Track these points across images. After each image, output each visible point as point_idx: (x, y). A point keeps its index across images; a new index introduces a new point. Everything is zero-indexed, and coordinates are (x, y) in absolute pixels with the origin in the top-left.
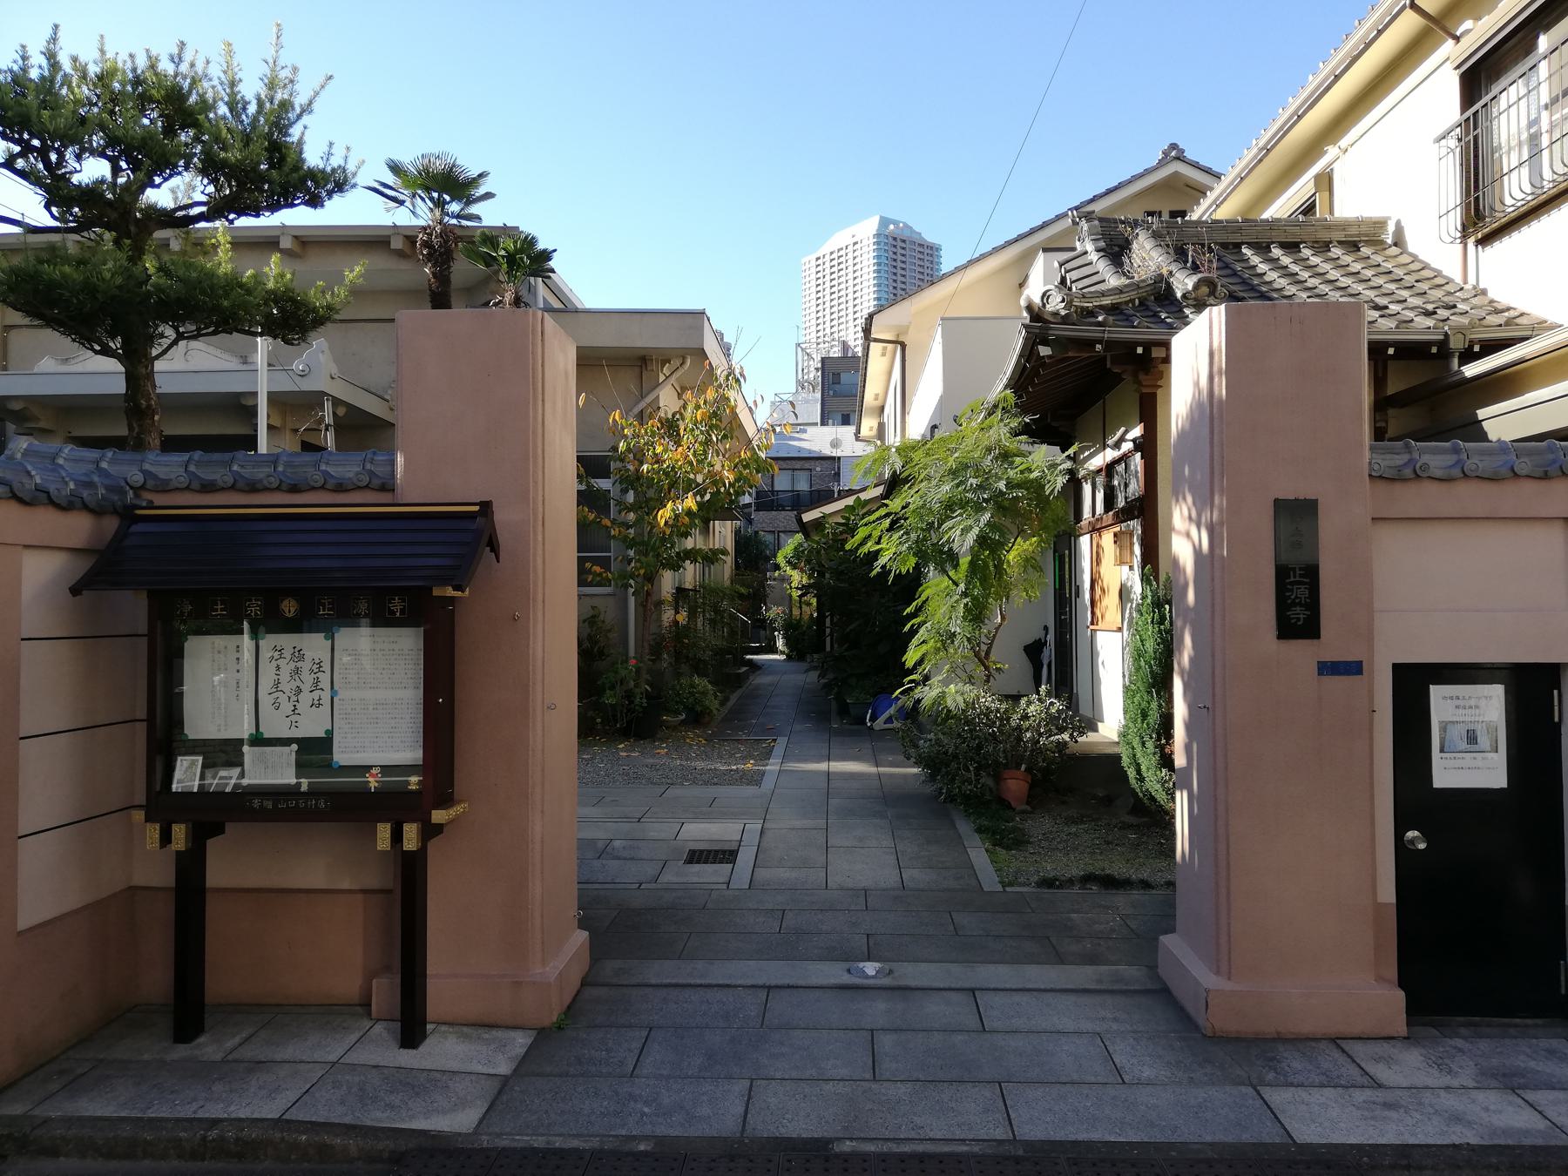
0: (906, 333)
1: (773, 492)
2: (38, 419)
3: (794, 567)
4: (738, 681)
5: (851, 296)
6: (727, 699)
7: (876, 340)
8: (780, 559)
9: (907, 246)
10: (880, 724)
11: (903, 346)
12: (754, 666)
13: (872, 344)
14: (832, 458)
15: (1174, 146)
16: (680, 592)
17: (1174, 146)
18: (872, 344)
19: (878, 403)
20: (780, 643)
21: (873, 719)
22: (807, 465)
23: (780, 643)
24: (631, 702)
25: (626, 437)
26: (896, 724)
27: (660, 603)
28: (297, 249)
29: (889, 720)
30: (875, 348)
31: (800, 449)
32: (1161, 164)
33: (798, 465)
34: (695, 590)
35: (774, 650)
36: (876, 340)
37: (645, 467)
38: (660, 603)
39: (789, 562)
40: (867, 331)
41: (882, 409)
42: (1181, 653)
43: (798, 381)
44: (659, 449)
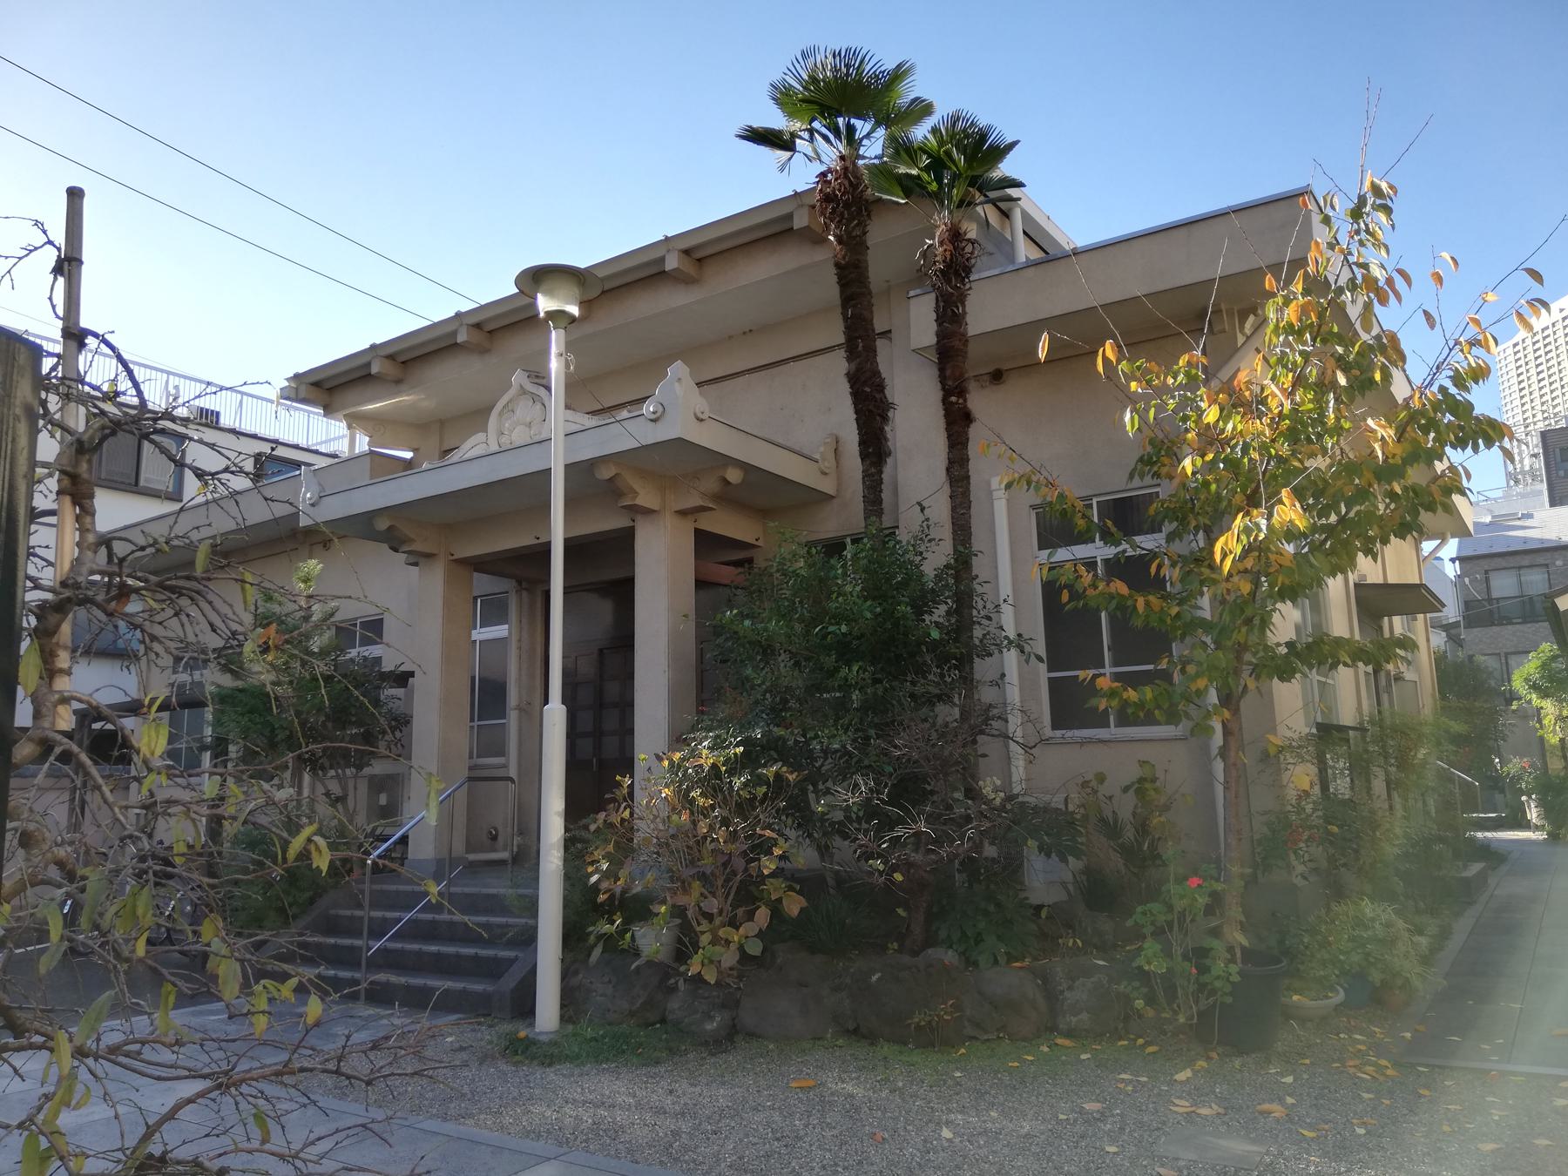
1: (1490, 600)
2: (411, 541)
3: (1545, 694)
4: (1467, 892)
6: (1445, 934)
8: (1518, 684)
12: (1492, 855)
16: (1328, 733)
20: (1533, 814)
22: (1540, 559)
23: (1533, 814)
24: (1203, 970)
25: (1132, 399)
27: (1270, 759)
28: (689, 268)
31: (1525, 540)
33: (1526, 561)
34: (1361, 729)
35: (1524, 824)
37: (1187, 464)
38: (1270, 759)
39: (1535, 687)
43: (1508, 475)
44: (1211, 415)
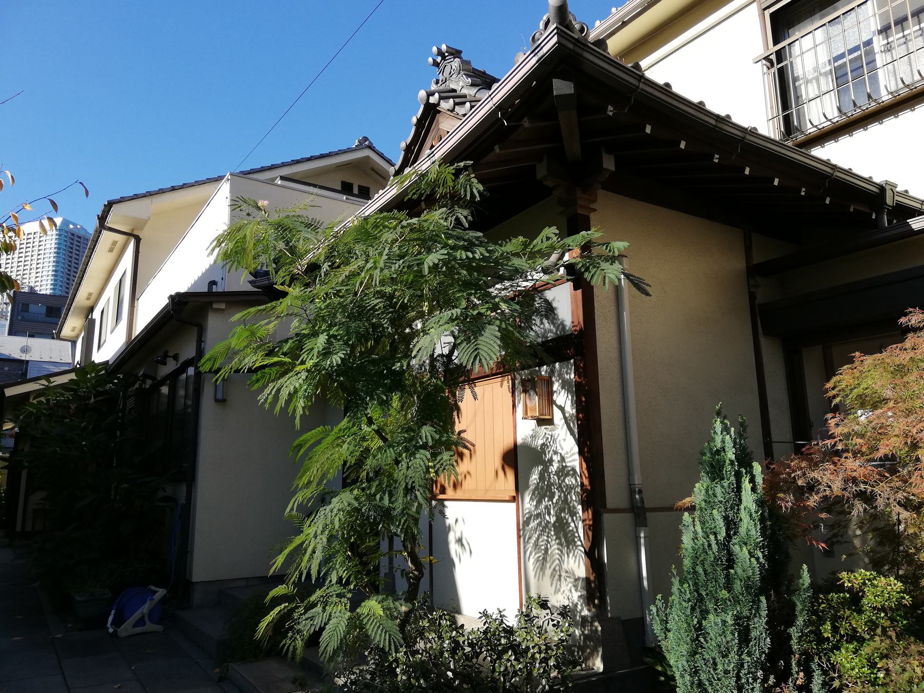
0: (142, 229)
5: (37, 244)
7: (111, 229)
9: (82, 241)
10: (127, 628)
11: (138, 240)
13: (104, 232)
14: (22, 361)
15: (365, 139)
17: (365, 139)
18: (104, 232)
19: (89, 303)
21: (118, 623)
26: (149, 627)
29: (141, 622)
30: (107, 237)
32: (359, 148)
36: (111, 229)
40: (102, 219)
41: (91, 309)
42: (799, 31)
